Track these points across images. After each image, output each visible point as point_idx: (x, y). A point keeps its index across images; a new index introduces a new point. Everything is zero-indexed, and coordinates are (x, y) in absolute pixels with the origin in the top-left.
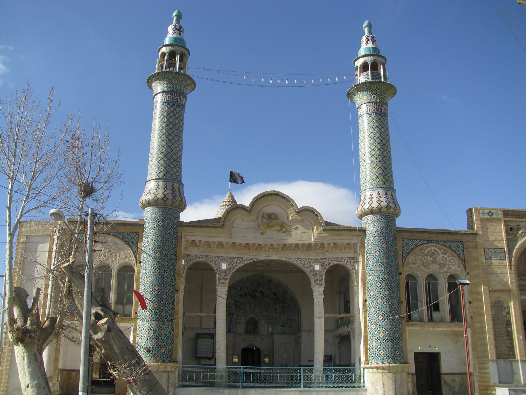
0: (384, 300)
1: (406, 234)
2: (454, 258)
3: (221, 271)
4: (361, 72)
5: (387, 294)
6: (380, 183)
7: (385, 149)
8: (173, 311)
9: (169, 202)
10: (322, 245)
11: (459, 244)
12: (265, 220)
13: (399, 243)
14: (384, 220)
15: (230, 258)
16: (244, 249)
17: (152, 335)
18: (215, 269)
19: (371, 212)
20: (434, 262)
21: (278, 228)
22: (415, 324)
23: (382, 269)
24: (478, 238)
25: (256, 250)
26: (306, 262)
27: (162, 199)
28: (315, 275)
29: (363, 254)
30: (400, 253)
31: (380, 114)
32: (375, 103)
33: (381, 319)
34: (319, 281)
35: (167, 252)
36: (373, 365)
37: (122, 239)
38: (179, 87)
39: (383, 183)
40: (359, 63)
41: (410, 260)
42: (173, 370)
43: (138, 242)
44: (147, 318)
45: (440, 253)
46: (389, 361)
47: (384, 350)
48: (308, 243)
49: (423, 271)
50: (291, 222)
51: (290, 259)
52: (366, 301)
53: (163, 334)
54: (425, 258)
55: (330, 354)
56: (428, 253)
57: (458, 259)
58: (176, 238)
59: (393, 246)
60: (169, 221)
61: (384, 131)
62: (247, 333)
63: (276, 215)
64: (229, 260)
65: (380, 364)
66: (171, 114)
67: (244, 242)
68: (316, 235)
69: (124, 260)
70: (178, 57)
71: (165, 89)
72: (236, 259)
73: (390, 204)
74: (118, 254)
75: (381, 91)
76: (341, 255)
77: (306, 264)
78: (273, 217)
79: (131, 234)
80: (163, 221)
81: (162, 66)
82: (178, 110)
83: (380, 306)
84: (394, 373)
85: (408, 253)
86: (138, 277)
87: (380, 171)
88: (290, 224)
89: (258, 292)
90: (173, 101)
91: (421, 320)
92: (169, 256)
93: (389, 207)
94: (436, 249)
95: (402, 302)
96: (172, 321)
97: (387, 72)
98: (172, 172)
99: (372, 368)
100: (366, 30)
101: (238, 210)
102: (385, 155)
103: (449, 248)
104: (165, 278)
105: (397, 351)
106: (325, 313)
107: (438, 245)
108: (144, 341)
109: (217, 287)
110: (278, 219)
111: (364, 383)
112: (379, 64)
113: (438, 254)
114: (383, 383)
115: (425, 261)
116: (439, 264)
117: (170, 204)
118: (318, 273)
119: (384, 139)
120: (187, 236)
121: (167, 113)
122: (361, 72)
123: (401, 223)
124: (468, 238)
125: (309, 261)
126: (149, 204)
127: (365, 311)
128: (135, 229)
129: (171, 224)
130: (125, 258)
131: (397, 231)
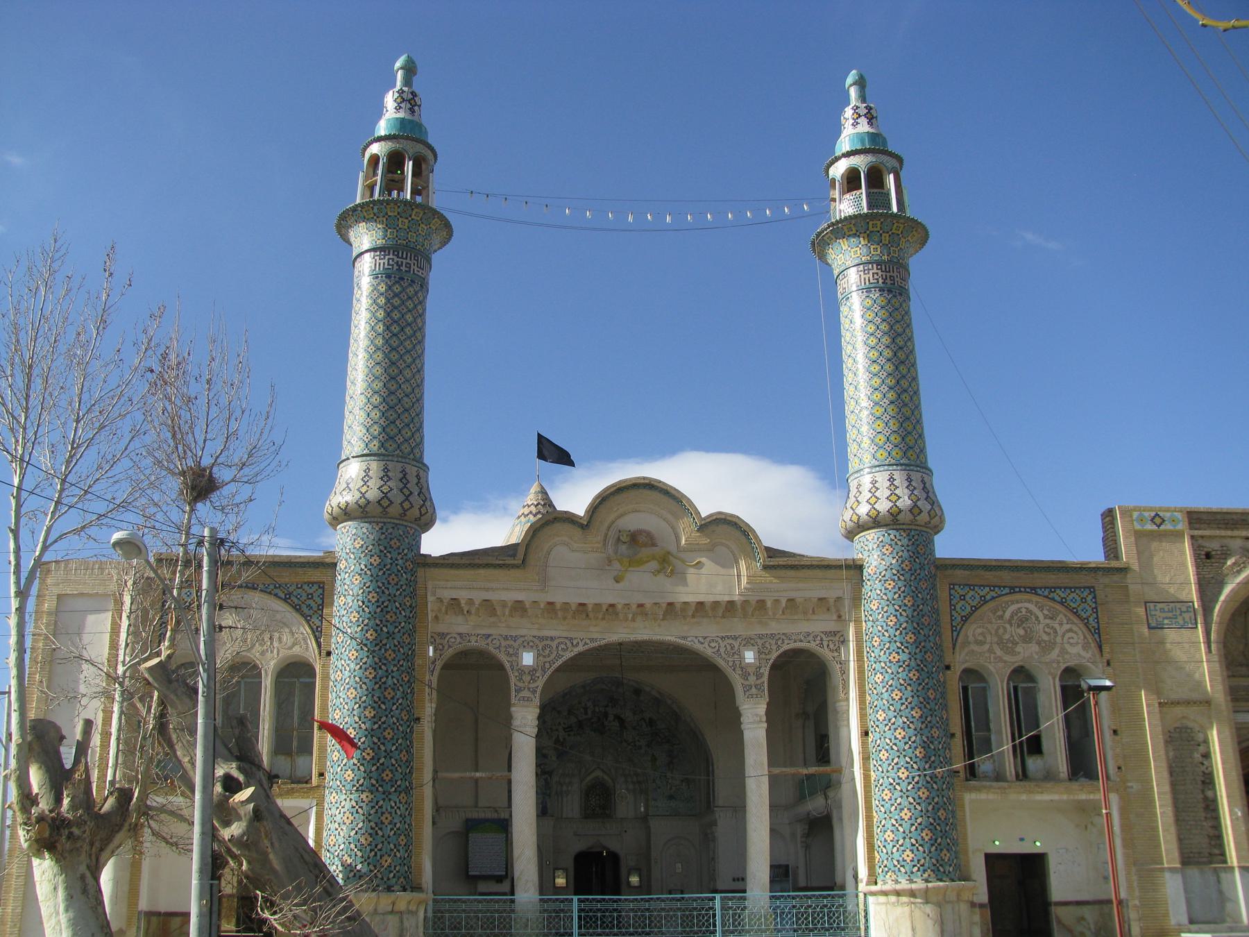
0: (911, 732)
1: (959, 572)
2: (1075, 628)
3: (522, 671)
4: (843, 193)
5: (917, 716)
6: (894, 453)
7: (904, 372)
8: (409, 766)
9: (395, 510)
10: (761, 604)
11: (1085, 594)
12: (623, 548)
13: (943, 594)
14: (905, 541)
15: (542, 639)
16: (574, 617)
17: (361, 825)
18: (507, 665)
19: (875, 522)
21: (654, 565)
22: (985, 787)
23: (904, 657)
24: (1130, 578)
25: (603, 619)
26: (722, 645)
27: (379, 502)
28: (745, 675)
29: (858, 621)
30: (945, 619)
31: (890, 291)
32: (878, 263)
33: (903, 777)
34: (754, 690)
35: (391, 628)
36: (889, 886)
37: (285, 600)
38: (412, 237)
39: (901, 454)
40: (839, 170)
41: (970, 633)
42: (413, 907)
43: (322, 605)
44: (348, 787)
45: (1041, 617)
46: (926, 875)
47: (912, 851)
48: (727, 598)
49: (1001, 660)
50: (685, 550)
51: (684, 638)
52: (866, 734)
53: (386, 822)
54: (1005, 628)
55: (783, 862)
56: (1012, 617)
57: (1084, 629)
58: (413, 595)
59: (929, 602)
60: (395, 555)
61: (900, 330)
62: (586, 817)
63: (649, 535)
64: (541, 645)
65: (904, 885)
66: (396, 302)
67: (574, 600)
68: (744, 580)
69: (290, 648)
70: (409, 166)
71: (380, 242)
72: (556, 642)
73: (919, 503)
74: (276, 635)
75: (892, 237)
76: (804, 627)
77: (722, 650)
78: (642, 539)
79: (305, 587)
80: (382, 555)
81: (371, 188)
82: (411, 291)
83: (901, 745)
84: (939, 905)
85: (965, 619)
86: (325, 688)
87: (893, 425)
88: (681, 555)
89: (611, 718)
90: (399, 270)
91: (999, 777)
92: (398, 636)
93: (916, 511)
94: (1031, 607)
96: (408, 790)
97: (905, 192)
98: (400, 439)
99: (885, 893)
100: (853, 92)
101: (558, 526)
102: (905, 386)
103: (1062, 603)
104: (389, 690)
105: (945, 851)
106: (770, 764)
107: (1035, 598)
108: (341, 840)
109: (513, 709)
110: (654, 545)
111: (867, 928)
112: (885, 172)
113: (1037, 618)
114: (913, 929)
115: (1007, 636)
116: (1039, 643)
117: (398, 513)
118: (750, 670)
119: (901, 348)
120: (440, 589)
121: (386, 298)
122: (843, 193)
123: (946, 546)
124: (1106, 580)
125: (731, 641)
126: (346, 514)
127: (866, 758)
128: (316, 576)
129: (400, 562)
130: (294, 644)
131: (937, 567)
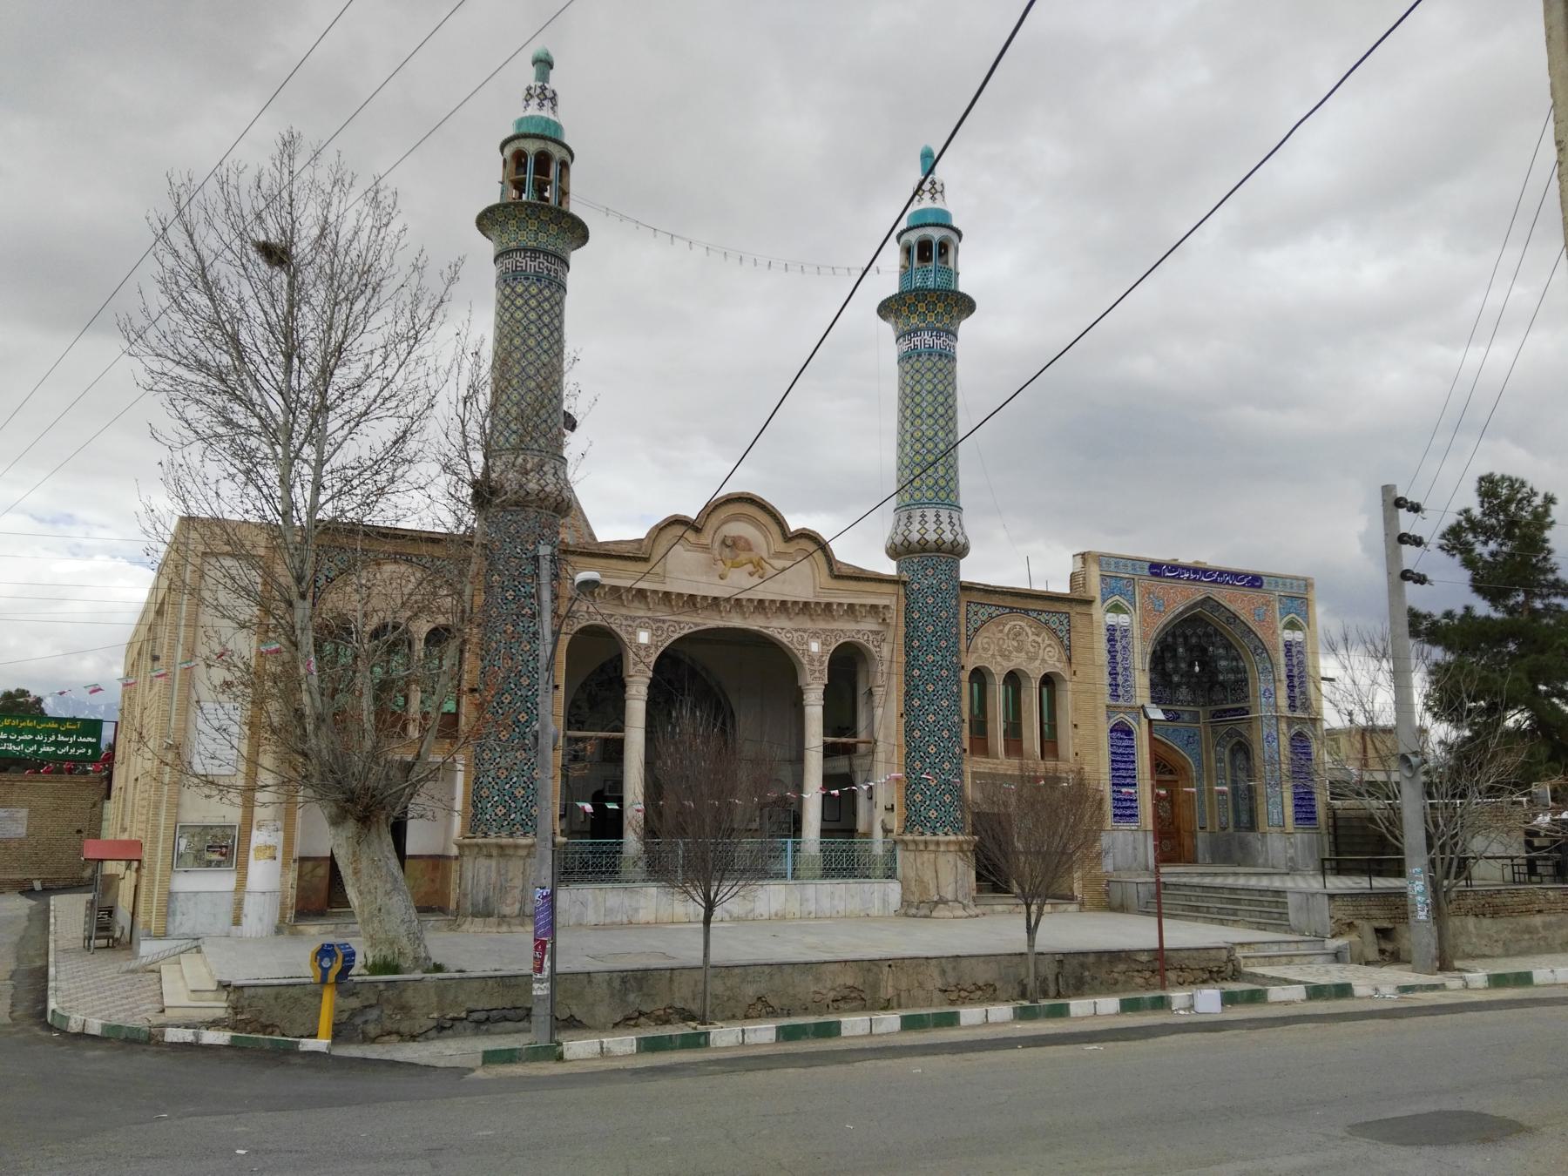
3: (639, 646)
13: (963, 610)
20: (1019, 649)
30: (963, 630)
62: (604, 760)
63: (747, 541)
67: (687, 591)
78: (742, 544)
85: (976, 630)
95: (556, 687)
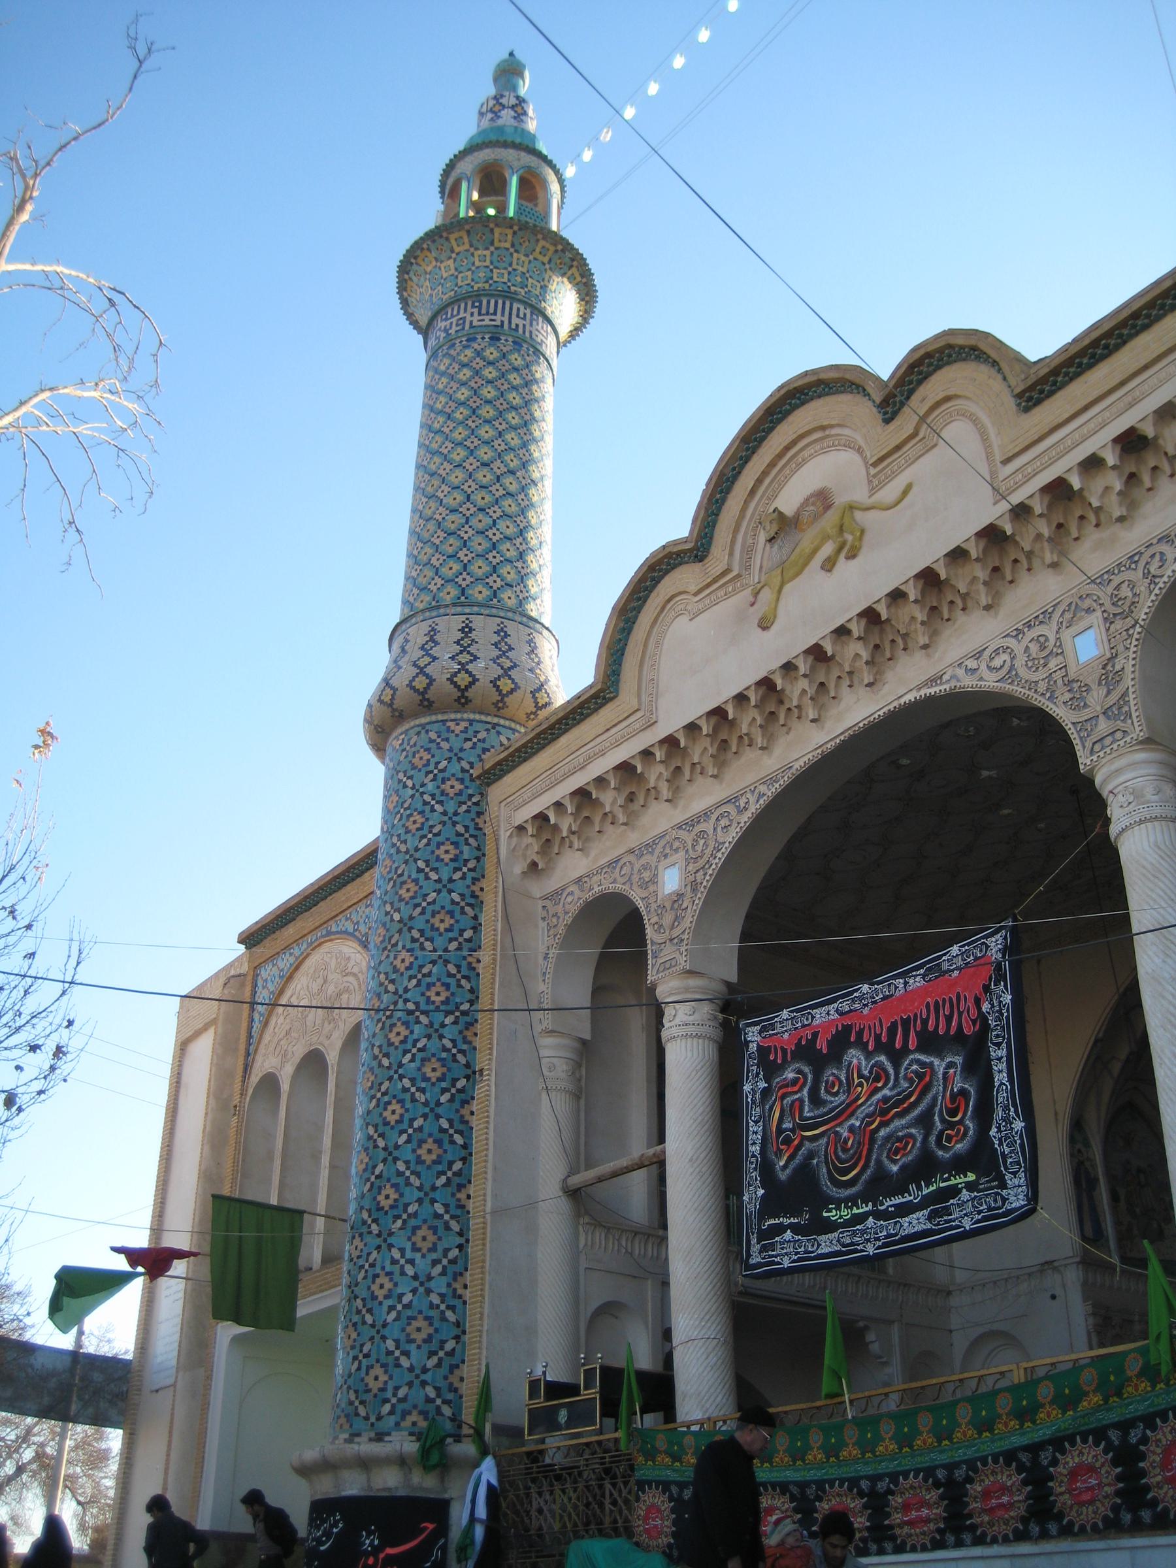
15: (691, 823)
26: (1019, 649)
51: (934, 680)
77: (1020, 663)
101: (667, 586)
118: (1092, 680)
